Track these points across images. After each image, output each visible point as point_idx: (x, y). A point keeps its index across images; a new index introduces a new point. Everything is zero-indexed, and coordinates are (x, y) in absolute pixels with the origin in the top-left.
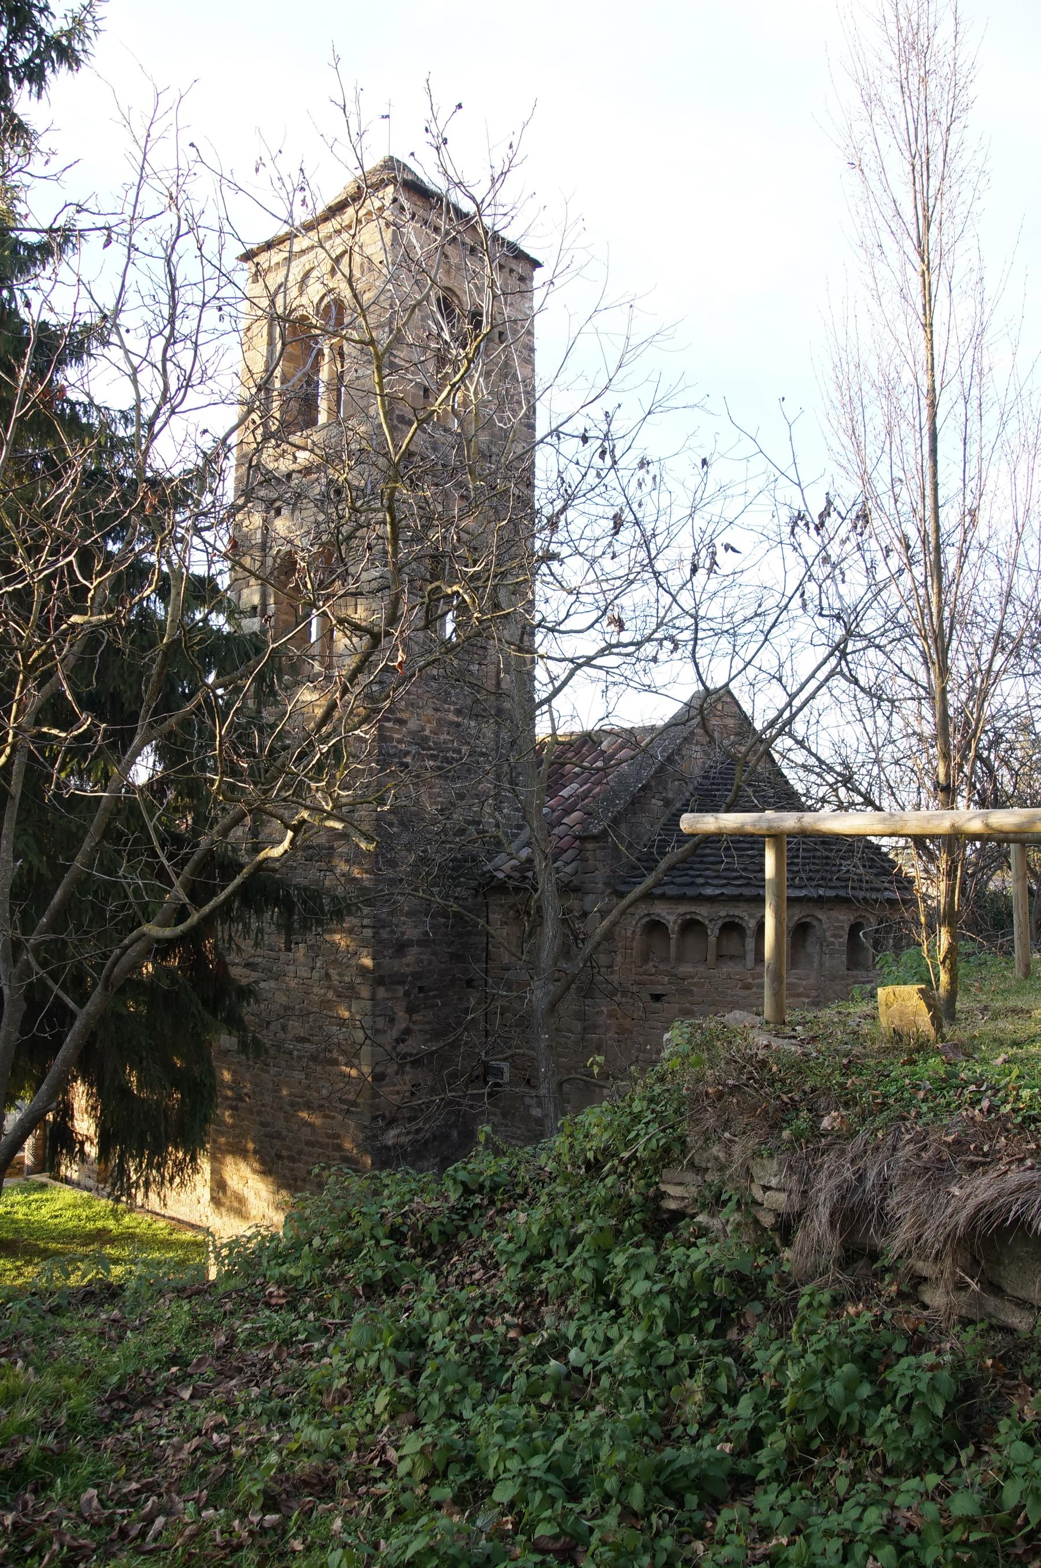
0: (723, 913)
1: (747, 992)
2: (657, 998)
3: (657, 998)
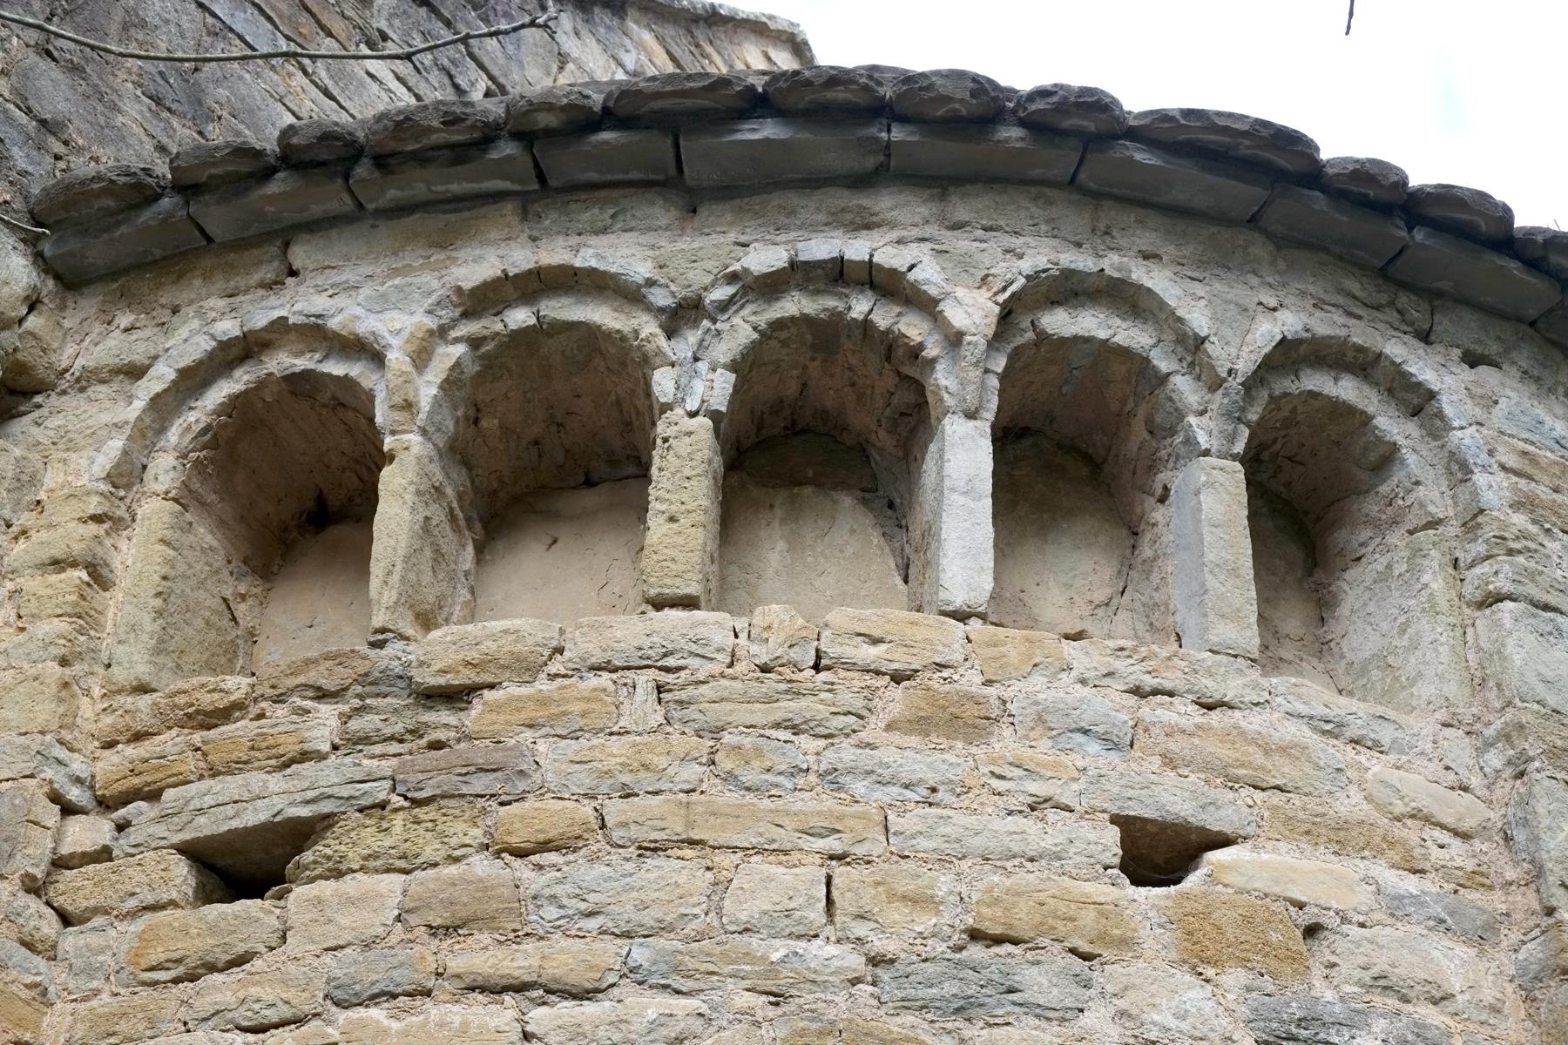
0: (765, 258)
3: (243, 868)
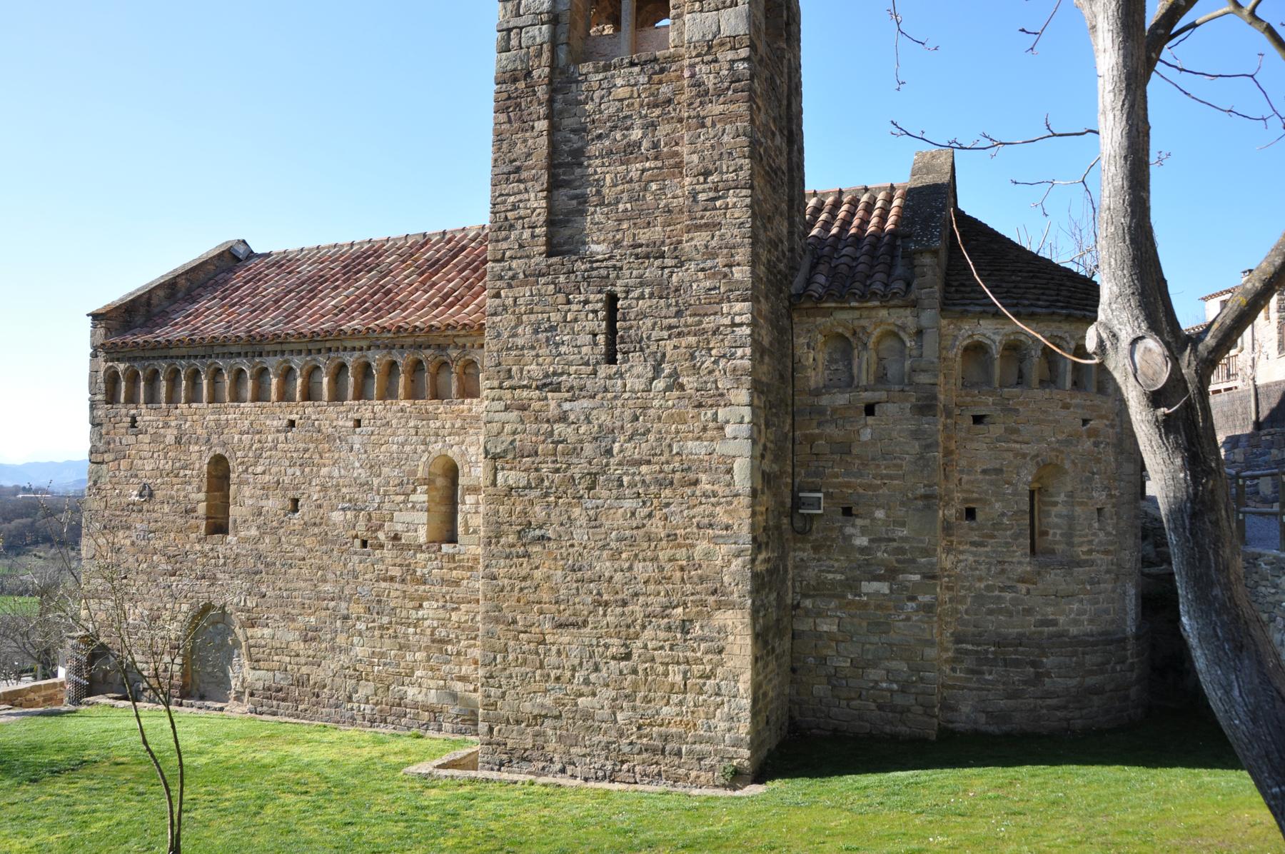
1: (1064, 413)
2: (978, 420)
3: (978, 420)
